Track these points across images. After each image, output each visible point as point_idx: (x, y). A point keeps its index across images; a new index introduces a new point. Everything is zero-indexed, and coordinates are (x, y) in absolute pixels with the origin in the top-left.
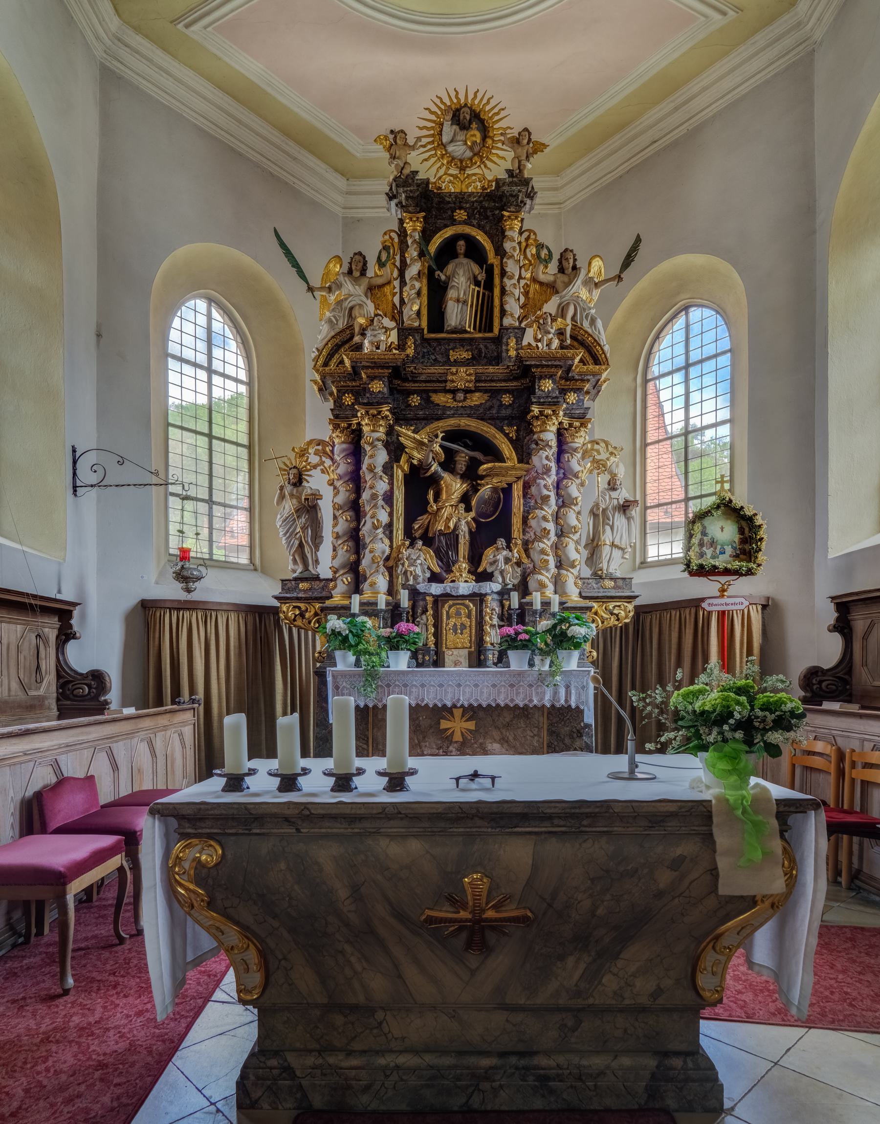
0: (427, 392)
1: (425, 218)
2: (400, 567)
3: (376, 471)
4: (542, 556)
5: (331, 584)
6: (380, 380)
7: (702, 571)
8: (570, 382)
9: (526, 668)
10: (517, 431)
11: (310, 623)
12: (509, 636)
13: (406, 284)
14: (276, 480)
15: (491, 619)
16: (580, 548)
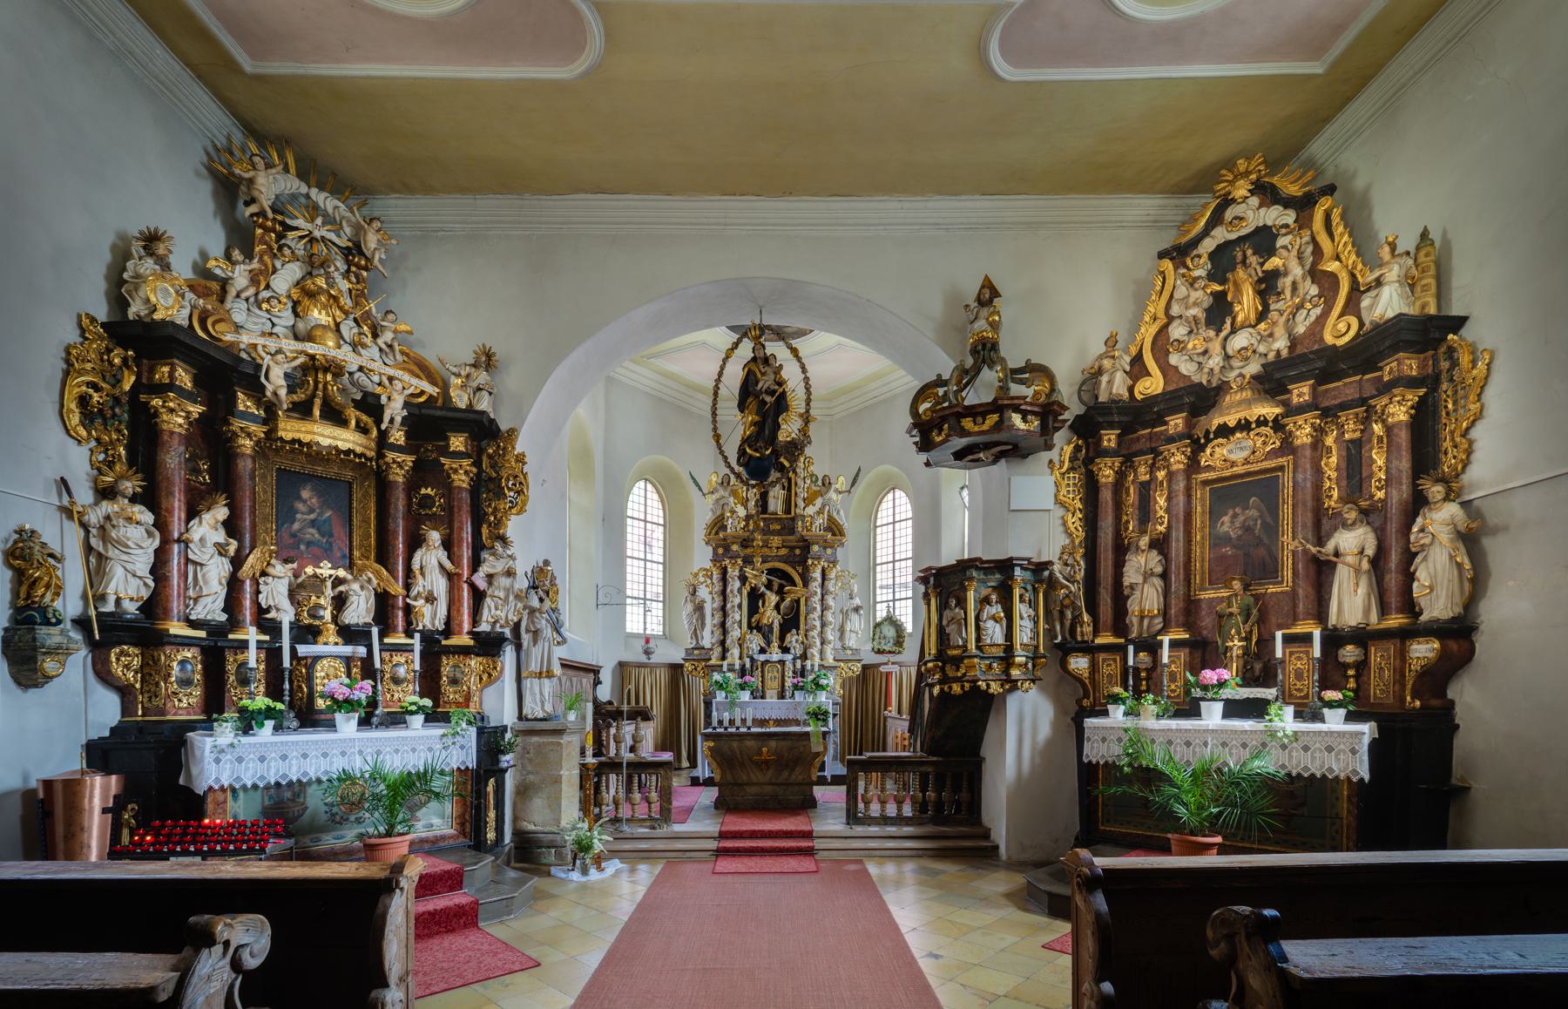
7: (879, 652)
8: (826, 545)
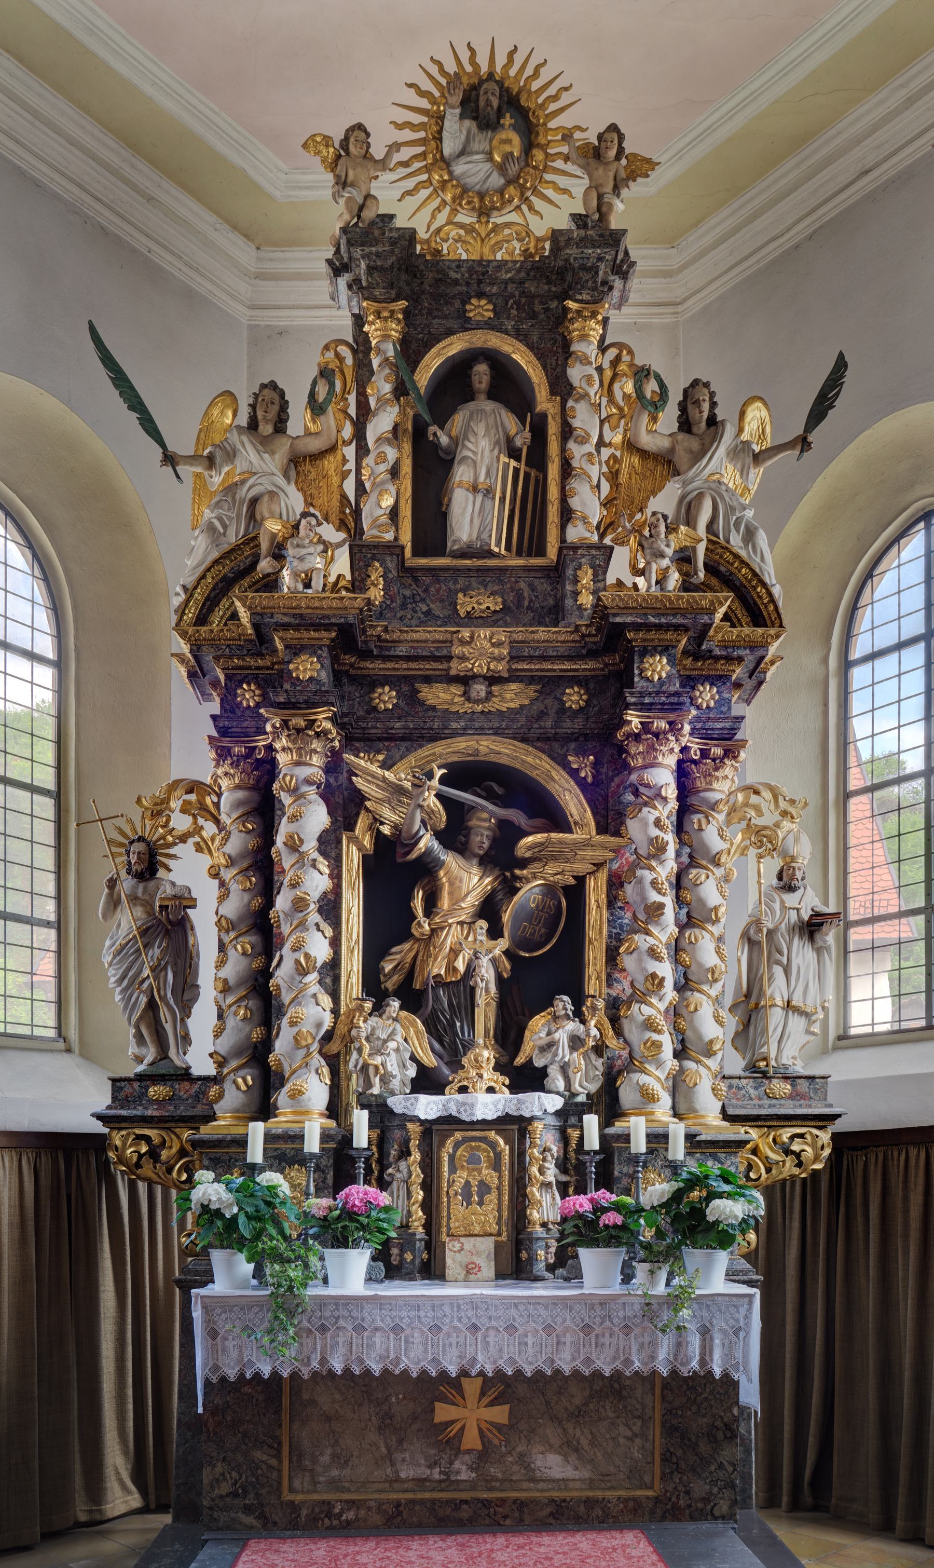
0: (409, 680)
1: (407, 312)
2: (355, 1055)
3: (303, 849)
4: (648, 1035)
5: (213, 1091)
6: (313, 654)
8: (705, 662)
9: (616, 1288)
10: (595, 765)
11: (169, 1170)
12: (580, 1216)
13: (368, 452)
14: (106, 865)
15: (542, 1171)
16: (724, 1013)
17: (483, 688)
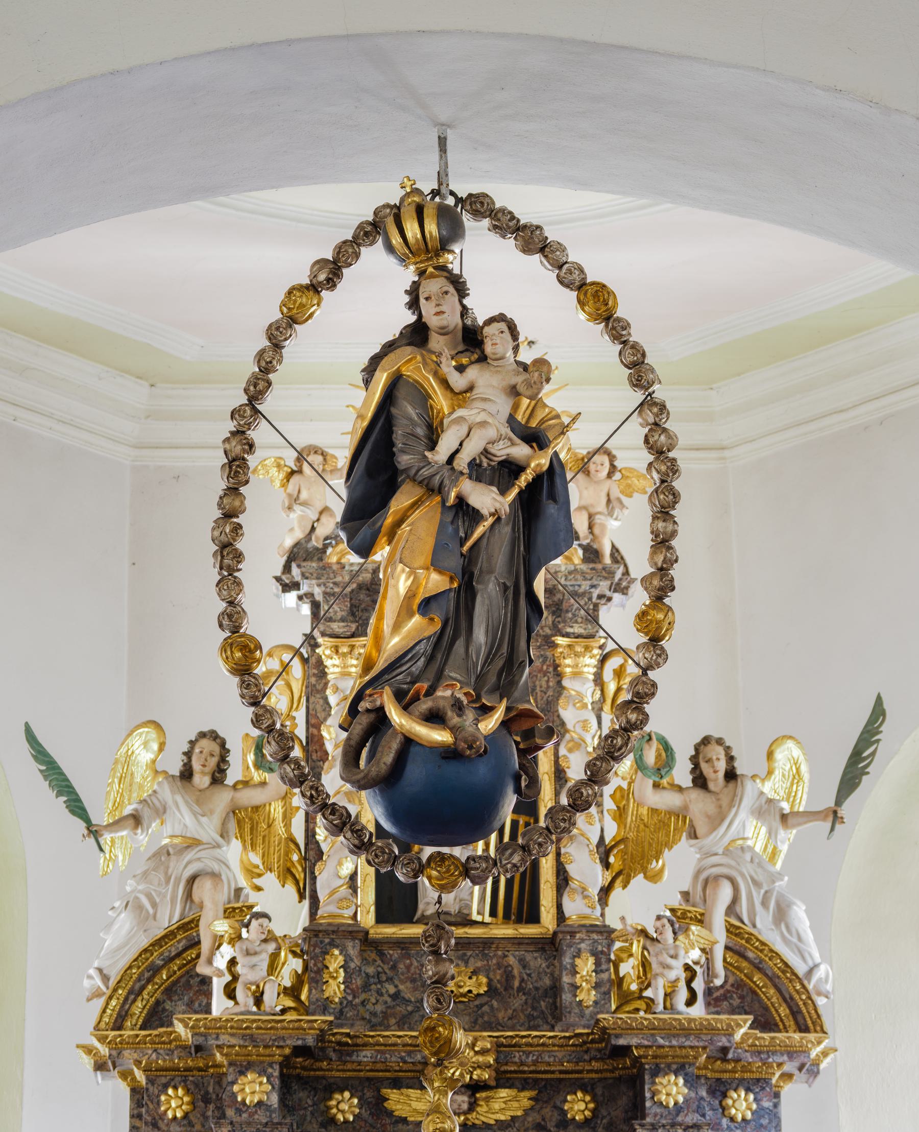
6: (262, 1072)
17: (466, 1098)
